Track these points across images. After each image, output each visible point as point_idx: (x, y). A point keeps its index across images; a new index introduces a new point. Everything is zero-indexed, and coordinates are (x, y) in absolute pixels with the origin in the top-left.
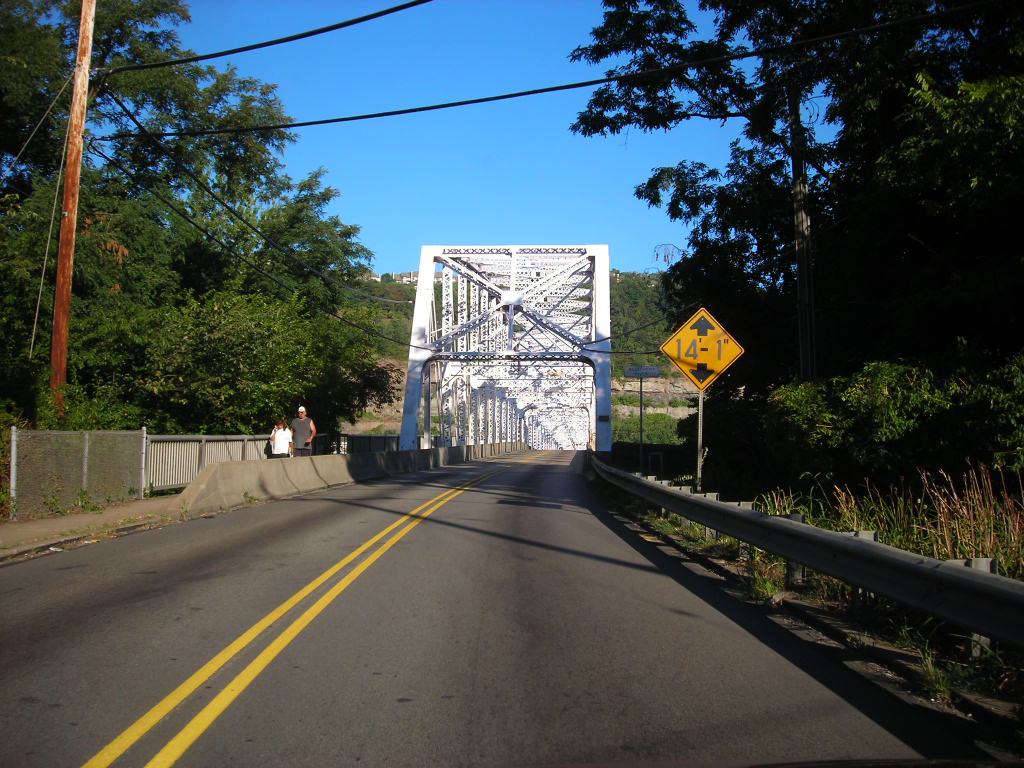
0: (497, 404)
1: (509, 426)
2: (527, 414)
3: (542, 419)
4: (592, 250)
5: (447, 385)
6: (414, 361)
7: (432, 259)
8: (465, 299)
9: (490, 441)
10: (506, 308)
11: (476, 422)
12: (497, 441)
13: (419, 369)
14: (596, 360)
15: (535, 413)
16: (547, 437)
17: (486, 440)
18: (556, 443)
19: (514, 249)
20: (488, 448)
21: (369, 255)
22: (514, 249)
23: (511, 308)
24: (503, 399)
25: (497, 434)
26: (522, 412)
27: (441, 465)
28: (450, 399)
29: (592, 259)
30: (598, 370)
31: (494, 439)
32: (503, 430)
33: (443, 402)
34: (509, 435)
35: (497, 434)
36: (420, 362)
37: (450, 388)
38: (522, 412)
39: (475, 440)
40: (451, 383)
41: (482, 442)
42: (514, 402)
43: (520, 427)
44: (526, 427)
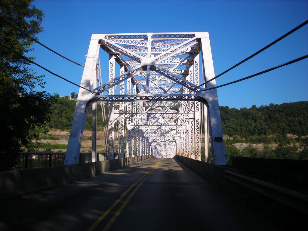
0: (140, 139)
1: (145, 149)
2: (152, 144)
3: (158, 146)
4: (198, 35)
5: (111, 124)
6: (81, 101)
7: (98, 41)
8: (130, 109)
9: (138, 155)
10: (144, 68)
11: (130, 148)
12: (141, 155)
13: (83, 107)
14: (208, 99)
15: (155, 144)
16: (159, 153)
17: (135, 155)
18: (161, 155)
19: (149, 35)
20: (136, 158)
21: (40, 14)
22: (149, 35)
23: (148, 67)
24: (143, 137)
25: (141, 152)
26: (151, 143)
27: (103, 172)
28: (113, 132)
29: (199, 40)
30: (210, 105)
31: (139, 155)
32: (143, 150)
33: (109, 134)
34: (145, 152)
35: (141, 152)
36: (85, 102)
37: (113, 126)
38: (151, 143)
39: (130, 155)
40: (113, 124)
41: (133, 156)
42: (147, 139)
43: (150, 149)
44: (152, 149)
